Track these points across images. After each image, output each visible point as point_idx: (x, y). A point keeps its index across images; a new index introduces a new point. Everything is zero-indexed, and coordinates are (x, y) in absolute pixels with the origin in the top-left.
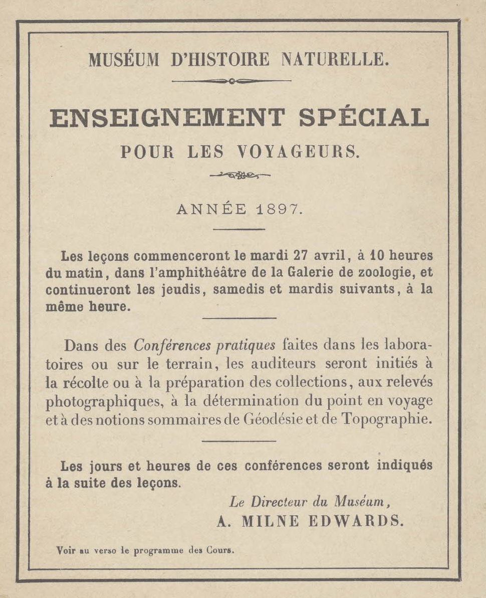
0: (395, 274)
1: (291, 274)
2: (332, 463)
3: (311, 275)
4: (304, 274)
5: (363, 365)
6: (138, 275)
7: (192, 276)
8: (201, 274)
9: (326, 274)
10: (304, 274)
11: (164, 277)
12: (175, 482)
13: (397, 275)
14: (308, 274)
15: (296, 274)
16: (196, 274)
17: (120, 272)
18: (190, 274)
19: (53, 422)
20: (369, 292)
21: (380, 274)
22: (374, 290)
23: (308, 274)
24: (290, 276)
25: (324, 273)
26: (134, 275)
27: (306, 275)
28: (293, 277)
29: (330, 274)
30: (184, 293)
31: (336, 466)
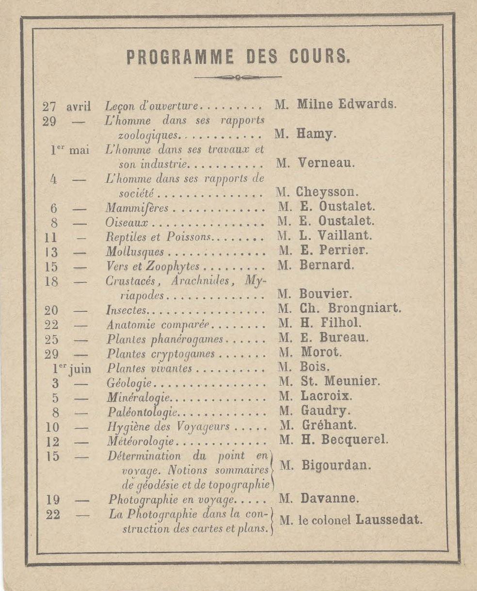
0: (362, 310)
1: (305, 412)
2: (390, 518)
3: (338, 297)
4: (354, 222)
5: (415, 521)
6: (335, 223)
7: (372, 311)
8: (344, 207)
9: (351, 252)
10: (354, 222)
11: (372, 108)
12: (389, 519)
13: (364, 311)
14: (358, 223)
15: (309, 412)
16: (345, 427)
17: (349, 464)
18: (328, 427)
19: (187, 486)
20: (326, 502)
21: (354, 324)
22: (332, 500)
23: (358, 223)
24: (307, 494)
25: (349, 251)
26: (355, 383)
27: (362, 384)
28: (306, 415)
29: (330, 106)
30: (375, 523)
31: (393, 520)
